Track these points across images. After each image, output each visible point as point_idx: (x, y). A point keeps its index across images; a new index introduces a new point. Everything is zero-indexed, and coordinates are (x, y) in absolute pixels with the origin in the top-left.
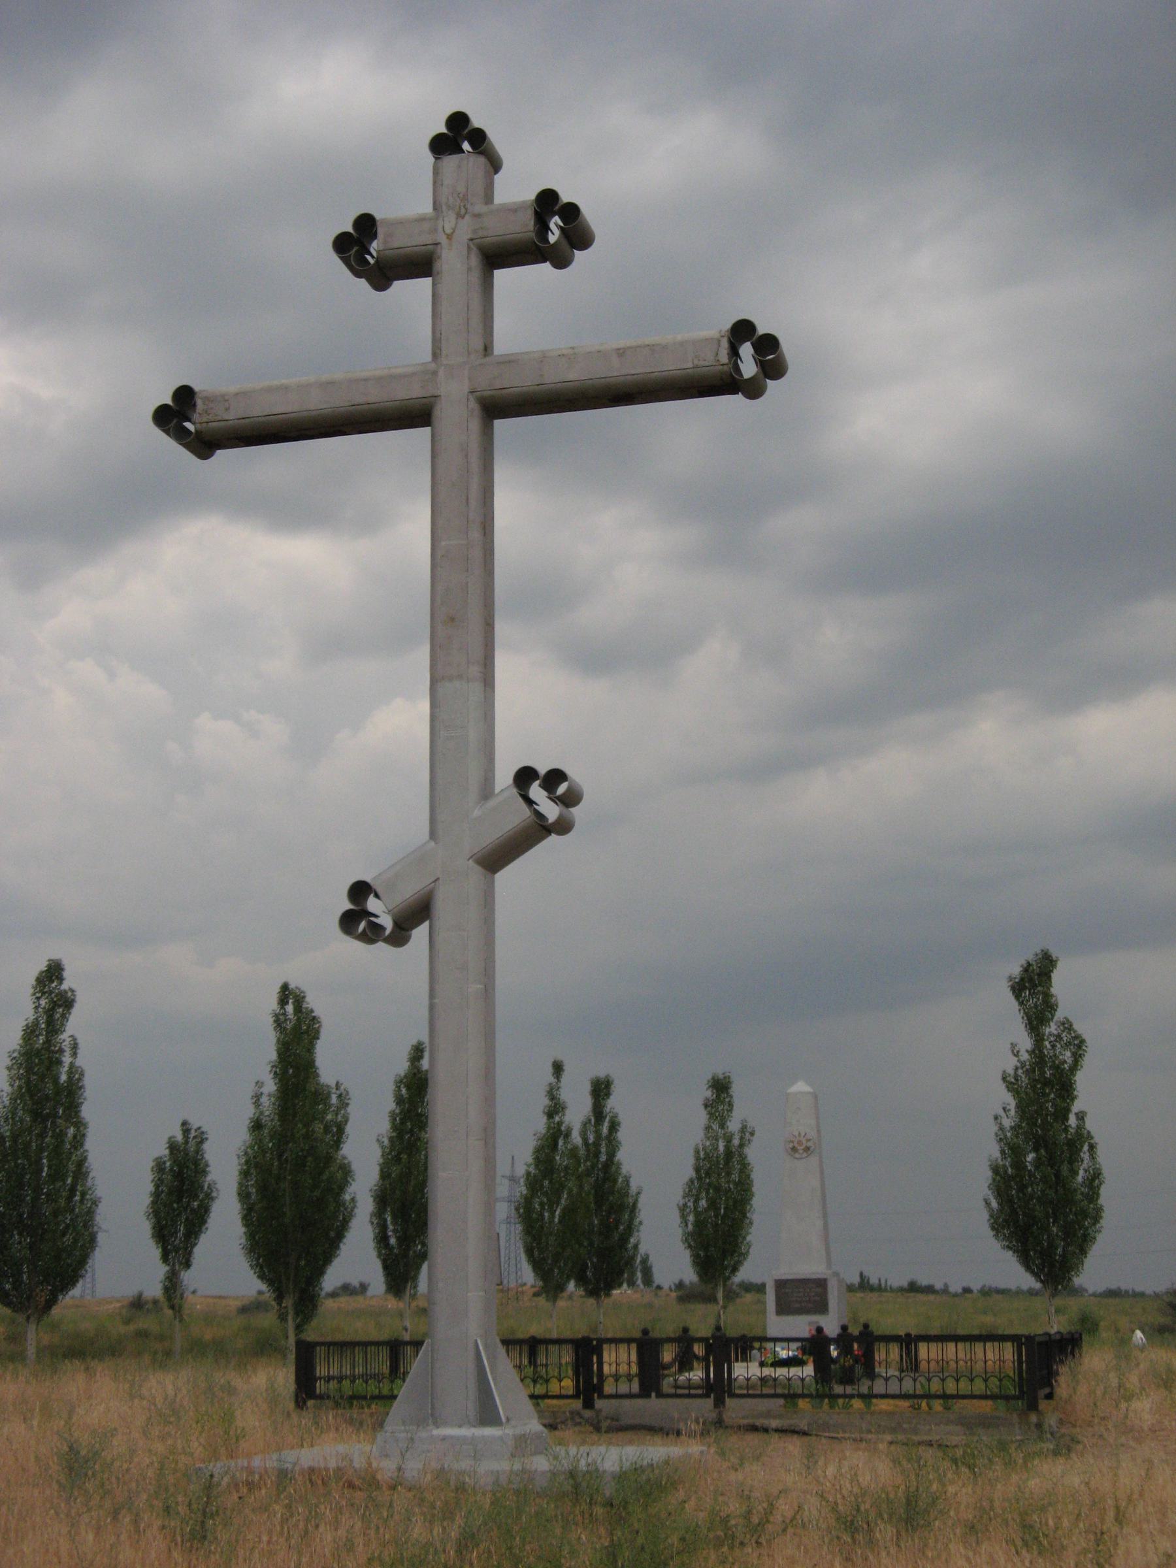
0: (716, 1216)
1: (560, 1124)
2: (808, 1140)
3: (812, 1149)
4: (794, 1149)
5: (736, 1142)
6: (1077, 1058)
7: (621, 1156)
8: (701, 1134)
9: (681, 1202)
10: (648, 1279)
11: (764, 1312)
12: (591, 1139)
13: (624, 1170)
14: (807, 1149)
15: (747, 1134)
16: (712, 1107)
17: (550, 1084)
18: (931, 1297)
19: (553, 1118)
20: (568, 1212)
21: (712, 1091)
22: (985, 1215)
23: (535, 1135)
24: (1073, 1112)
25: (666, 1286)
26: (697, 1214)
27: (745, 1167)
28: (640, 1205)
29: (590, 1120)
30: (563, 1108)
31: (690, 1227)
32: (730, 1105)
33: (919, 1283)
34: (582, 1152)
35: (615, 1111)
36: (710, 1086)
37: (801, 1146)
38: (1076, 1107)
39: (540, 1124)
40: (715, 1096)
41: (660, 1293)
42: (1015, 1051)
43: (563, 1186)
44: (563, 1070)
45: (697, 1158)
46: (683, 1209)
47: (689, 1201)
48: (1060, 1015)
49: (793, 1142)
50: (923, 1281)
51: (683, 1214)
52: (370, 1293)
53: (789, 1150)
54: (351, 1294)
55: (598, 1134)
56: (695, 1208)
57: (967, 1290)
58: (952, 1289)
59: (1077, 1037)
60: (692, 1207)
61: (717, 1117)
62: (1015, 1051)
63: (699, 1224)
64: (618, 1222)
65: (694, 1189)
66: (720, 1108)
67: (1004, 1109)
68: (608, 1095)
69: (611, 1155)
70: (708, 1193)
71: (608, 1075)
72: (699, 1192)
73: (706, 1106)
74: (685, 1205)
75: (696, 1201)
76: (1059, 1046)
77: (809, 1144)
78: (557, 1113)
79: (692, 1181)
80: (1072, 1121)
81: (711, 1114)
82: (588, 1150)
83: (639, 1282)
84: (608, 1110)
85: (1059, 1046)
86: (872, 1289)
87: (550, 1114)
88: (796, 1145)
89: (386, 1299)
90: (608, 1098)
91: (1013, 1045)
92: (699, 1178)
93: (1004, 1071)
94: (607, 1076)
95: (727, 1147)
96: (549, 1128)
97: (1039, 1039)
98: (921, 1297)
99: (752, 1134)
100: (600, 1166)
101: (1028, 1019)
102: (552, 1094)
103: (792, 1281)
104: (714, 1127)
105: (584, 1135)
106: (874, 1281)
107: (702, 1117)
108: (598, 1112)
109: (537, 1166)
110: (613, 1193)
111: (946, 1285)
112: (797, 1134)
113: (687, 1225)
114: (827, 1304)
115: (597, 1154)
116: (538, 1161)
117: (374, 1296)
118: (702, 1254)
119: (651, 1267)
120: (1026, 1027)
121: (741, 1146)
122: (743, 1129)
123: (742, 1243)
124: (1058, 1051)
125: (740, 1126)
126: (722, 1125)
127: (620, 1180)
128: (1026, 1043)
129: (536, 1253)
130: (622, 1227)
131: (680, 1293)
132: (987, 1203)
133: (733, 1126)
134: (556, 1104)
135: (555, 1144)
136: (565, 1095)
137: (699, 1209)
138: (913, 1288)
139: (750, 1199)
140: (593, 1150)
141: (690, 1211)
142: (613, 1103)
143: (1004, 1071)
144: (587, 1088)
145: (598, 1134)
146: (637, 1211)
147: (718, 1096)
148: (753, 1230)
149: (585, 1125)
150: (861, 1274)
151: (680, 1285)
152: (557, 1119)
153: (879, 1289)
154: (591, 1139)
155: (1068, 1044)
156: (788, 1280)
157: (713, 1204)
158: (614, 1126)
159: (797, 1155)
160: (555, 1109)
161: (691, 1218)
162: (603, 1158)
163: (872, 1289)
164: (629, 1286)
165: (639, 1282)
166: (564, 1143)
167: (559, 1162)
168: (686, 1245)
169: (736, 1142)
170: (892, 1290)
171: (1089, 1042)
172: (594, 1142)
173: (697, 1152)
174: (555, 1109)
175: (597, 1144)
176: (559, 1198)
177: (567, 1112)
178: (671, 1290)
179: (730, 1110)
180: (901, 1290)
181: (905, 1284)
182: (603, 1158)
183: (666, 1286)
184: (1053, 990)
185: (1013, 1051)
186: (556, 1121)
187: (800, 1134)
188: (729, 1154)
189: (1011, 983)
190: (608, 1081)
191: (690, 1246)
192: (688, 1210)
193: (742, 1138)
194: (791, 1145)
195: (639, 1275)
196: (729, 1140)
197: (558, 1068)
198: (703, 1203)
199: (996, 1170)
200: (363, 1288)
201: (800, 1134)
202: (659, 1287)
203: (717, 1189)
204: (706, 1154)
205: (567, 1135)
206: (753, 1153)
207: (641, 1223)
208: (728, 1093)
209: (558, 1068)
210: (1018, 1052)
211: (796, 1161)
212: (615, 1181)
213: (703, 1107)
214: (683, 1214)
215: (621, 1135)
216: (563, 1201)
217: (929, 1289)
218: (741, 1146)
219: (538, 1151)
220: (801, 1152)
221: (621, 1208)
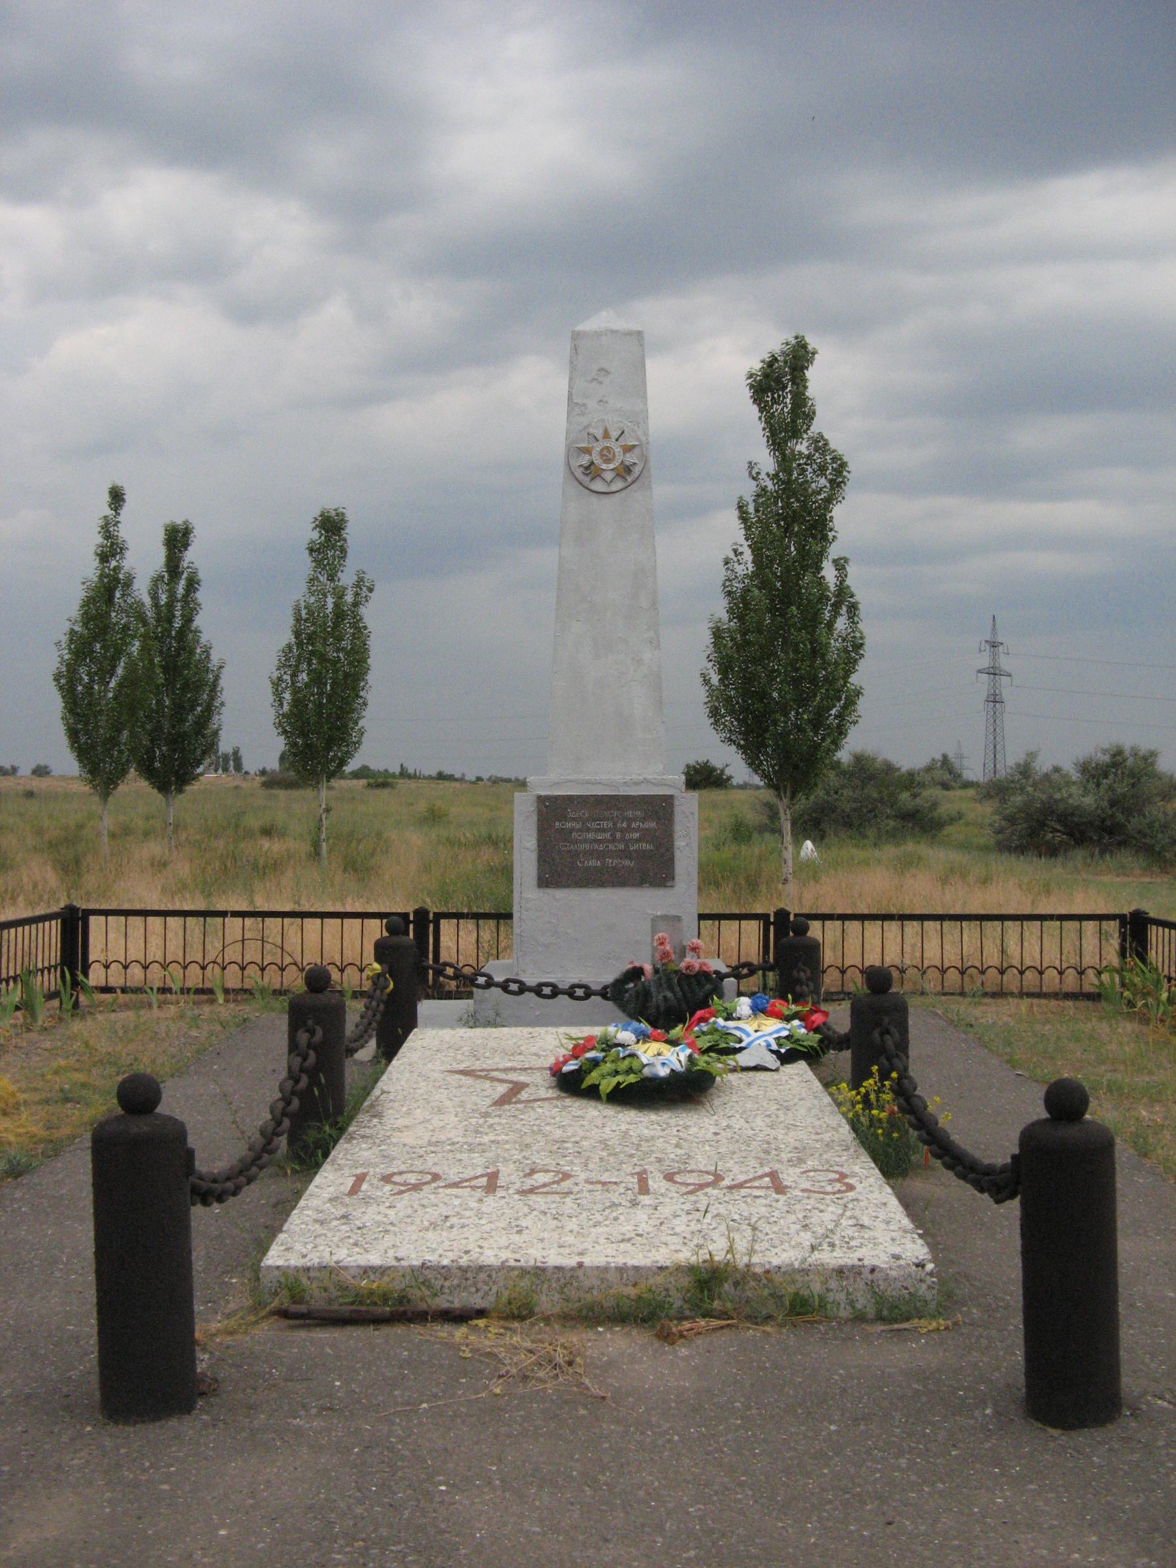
0: (321, 694)
1: (117, 569)
2: (628, 449)
3: (636, 471)
4: (591, 470)
5: (349, 598)
6: (837, 484)
7: (199, 621)
8: (303, 587)
9: (276, 674)
10: (238, 767)
11: (506, 872)
12: (163, 599)
13: (204, 639)
14: (625, 471)
15: (365, 589)
16: (319, 553)
17: (105, 517)
18: (453, 784)
19: (107, 561)
20: (129, 682)
21: (320, 532)
22: (702, 694)
23: (84, 583)
24: (830, 558)
25: (252, 773)
26: (296, 691)
27: (359, 631)
28: (222, 682)
29: (163, 577)
30: (121, 549)
31: (286, 708)
32: (343, 550)
33: (446, 773)
34: (150, 614)
35: (196, 565)
36: (317, 526)
37: (608, 461)
38: (834, 551)
39: (90, 569)
40: (323, 538)
41: (248, 777)
42: (754, 473)
43: (119, 653)
44: (123, 500)
45: (298, 619)
46: (277, 683)
47: (285, 673)
48: (816, 427)
49: (588, 451)
50: (448, 771)
51: (277, 690)
52: (20, 773)
53: (579, 473)
54: (4, 775)
55: (172, 594)
56: (293, 683)
57: (479, 779)
58: (467, 778)
59: (834, 459)
60: (289, 681)
61: (325, 566)
62: (754, 473)
63: (297, 703)
64: (193, 704)
65: (292, 659)
66: (330, 554)
67: (735, 551)
68: (186, 546)
69: (188, 620)
70: (310, 664)
71: (187, 521)
72: (299, 659)
73: (311, 550)
74: (280, 679)
75: (294, 675)
76: (810, 470)
77: (630, 458)
78: (114, 556)
79: (289, 647)
80: (829, 573)
81: (318, 563)
82: (158, 613)
83: (231, 768)
84: (185, 565)
85: (810, 470)
86: (409, 777)
87: (104, 557)
88: (598, 461)
89: (32, 779)
90: (186, 549)
91: (751, 466)
92: (300, 644)
93: (741, 498)
94: (186, 522)
95: (336, 605)
96: (101, 577)
97: (785, 460)
98: (447, 784)
99: (371, 590)
100: (173, 633)
101: (771, 431)
102: (108, 529)
103: (583, 800)
104: (321, 578)
105: (154, 597)
106: (411, 771)
107: (306, 564)
108: (173, 566)
109: (85, 624)
110: (187, 666)
111: (463, 775)
112: (599, 433)
113: (281, 705)
114: (672, 860)
115: (170, 619)
116: (87, 618)
117: (21, 777)
118: (300, 741)
119: (241, 757)
120: (768, 442)
121: (356, 604)
122: (359, 584)
123: (353, 728)
124: (809, 476)
125: (356, 578)
126: (331, 578)
127: (198, 651)
128: (767, 462)
129: (83, 739)
130: (199, 709)
131: (264, 779)
132: (706, 681)
133: (347, 578)
134: (112, 544)
135: (110, 600)
136: (125, 531)
137: (299, 685)
138: (441, 776)
139: (366, 673)
140: (165, 615)
141: (287, 687)
142: (191, 556)
143: (741, 498)
144: (161, 536)
145: (172, 594)
146: (219, 689)
147: (328, 539)
148: (368, 713)
149: (157, 581)
150: (402, 765)
151: (263, 772)
152: (114, 563)
153: (414, 777)
154: (163, 599)
155: (822, 469)
156: (570, 799)
157: (317, 679)
158: (193, 584)
159: (598, 486)
160: (111, 549)
161: (287, 696)
162: (177, 623)
163: (409, 777)
164: (223, 771)
165: (231, 768)
166: (123, 595)
167: (114, 621)
168: (280, 730)
169: (349, 598)
170: (425, 778)
171: (851, 467)
172: (167, 604)
173: (297, 610)
174: (111, 549)
175: (170, 605)
176: (114, 668)
177: (127, 554)
178: (256, 775)
179: (343, 558)
180: (430, 778)
181: (434, 773)
182: (177, 623)
183: (252, 773)
184: (809, 393)
185: (750, 473)
186: (112, 567)
187: (606, 435)
188: (339, 615)
189: (749, 381)
190: (187, 529)
191: (285, 732)
192: (284, 685)
193: (357, 594)
194: (585, 460)
195: (231, 763)
196: (340, 595)
197: (117, 497)
198: (304, 677)
199: (717, 633)
200: (14, 770)
201: (606, 435)
202: (247, 773)
203: (323, 658)
204: (310, 612)
205: (128, 583)
206: (369, 614)
207: (222, 704)
208: (340, 536)
209: (117, 497)
210: (758, 473)
211: (594, 499)
212: (192, 652)
213: (307, 552)
214: (277, 690)
215: (200, 596)
216: (120, 671)
217: (451, 778)
218: (356, 604)
219: (87, 603)
220: (609, 476)
221: (199, 686)
